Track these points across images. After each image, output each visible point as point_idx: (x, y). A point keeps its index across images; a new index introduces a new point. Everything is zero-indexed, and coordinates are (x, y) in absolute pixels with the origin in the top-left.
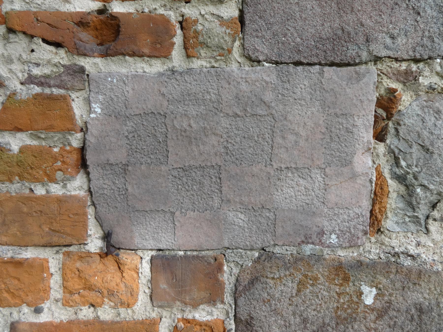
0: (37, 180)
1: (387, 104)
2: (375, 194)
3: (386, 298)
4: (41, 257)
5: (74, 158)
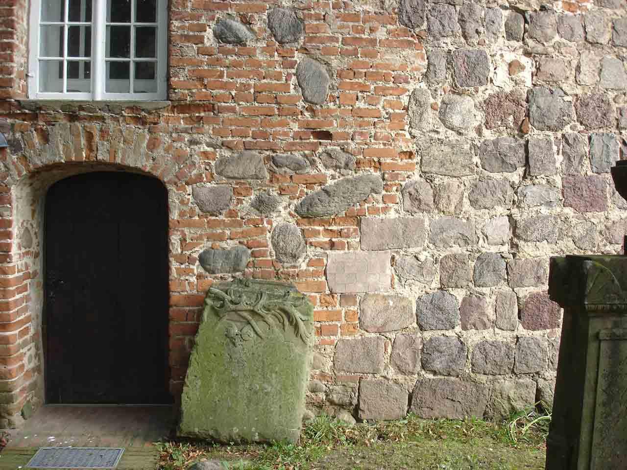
1: (393, 258)
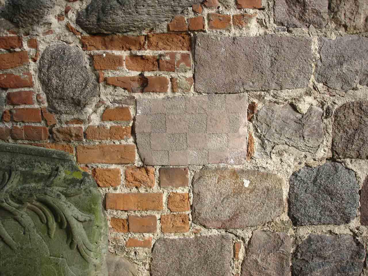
0: (116, 139)
1: (252, 107)
2: (248, 143)
3: (254, 185)
4: (117, 168)
5: (130, 130)
